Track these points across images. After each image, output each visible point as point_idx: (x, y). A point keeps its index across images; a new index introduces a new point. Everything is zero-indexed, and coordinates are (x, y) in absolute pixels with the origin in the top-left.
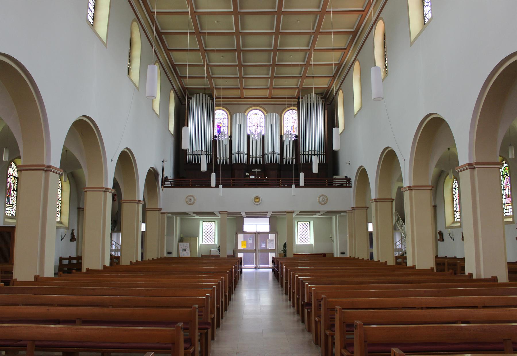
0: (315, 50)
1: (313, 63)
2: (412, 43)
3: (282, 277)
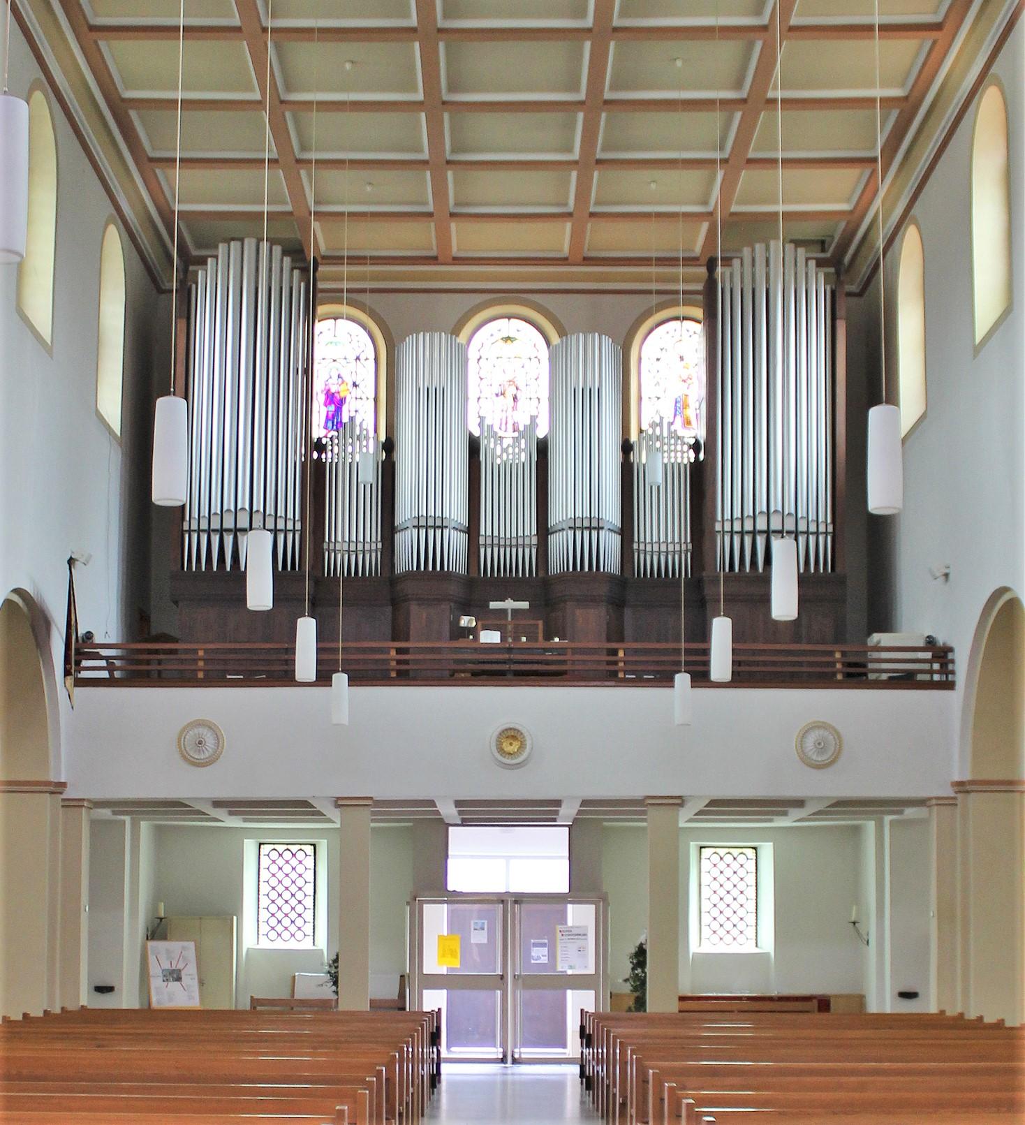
0: (792, 29)
1: (779, 94)
2: (977, 349)
3: (623, 1105)
